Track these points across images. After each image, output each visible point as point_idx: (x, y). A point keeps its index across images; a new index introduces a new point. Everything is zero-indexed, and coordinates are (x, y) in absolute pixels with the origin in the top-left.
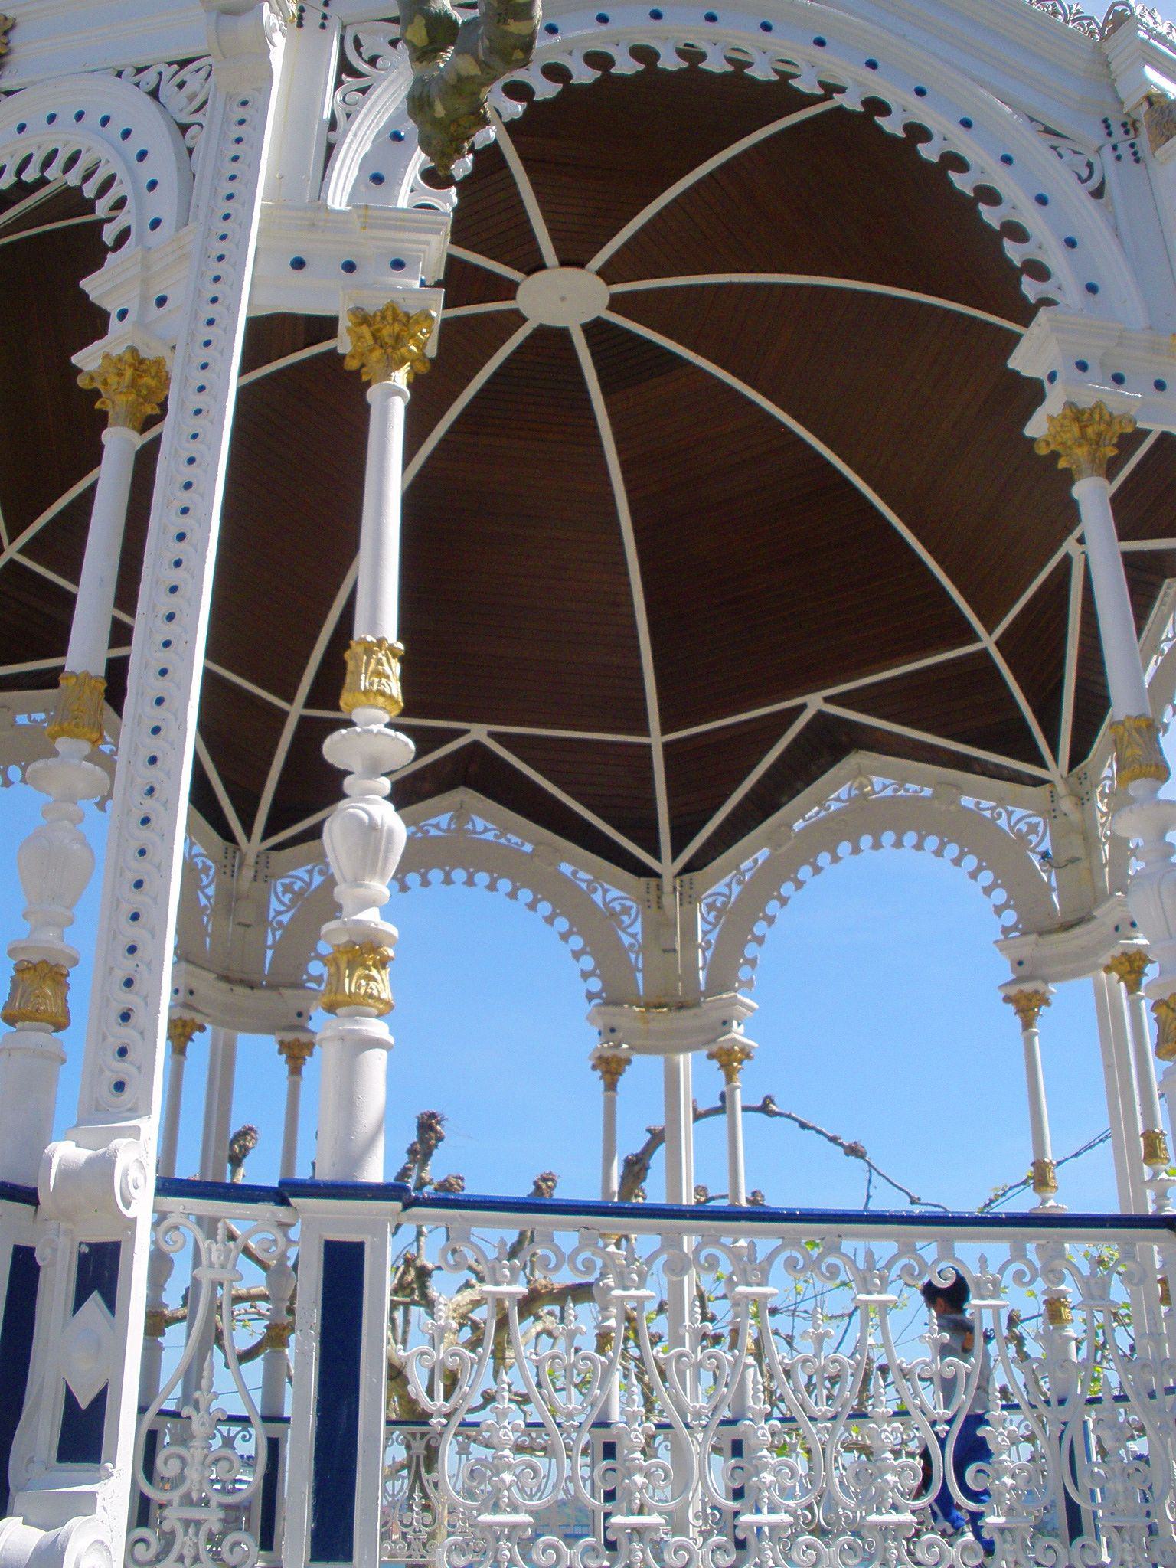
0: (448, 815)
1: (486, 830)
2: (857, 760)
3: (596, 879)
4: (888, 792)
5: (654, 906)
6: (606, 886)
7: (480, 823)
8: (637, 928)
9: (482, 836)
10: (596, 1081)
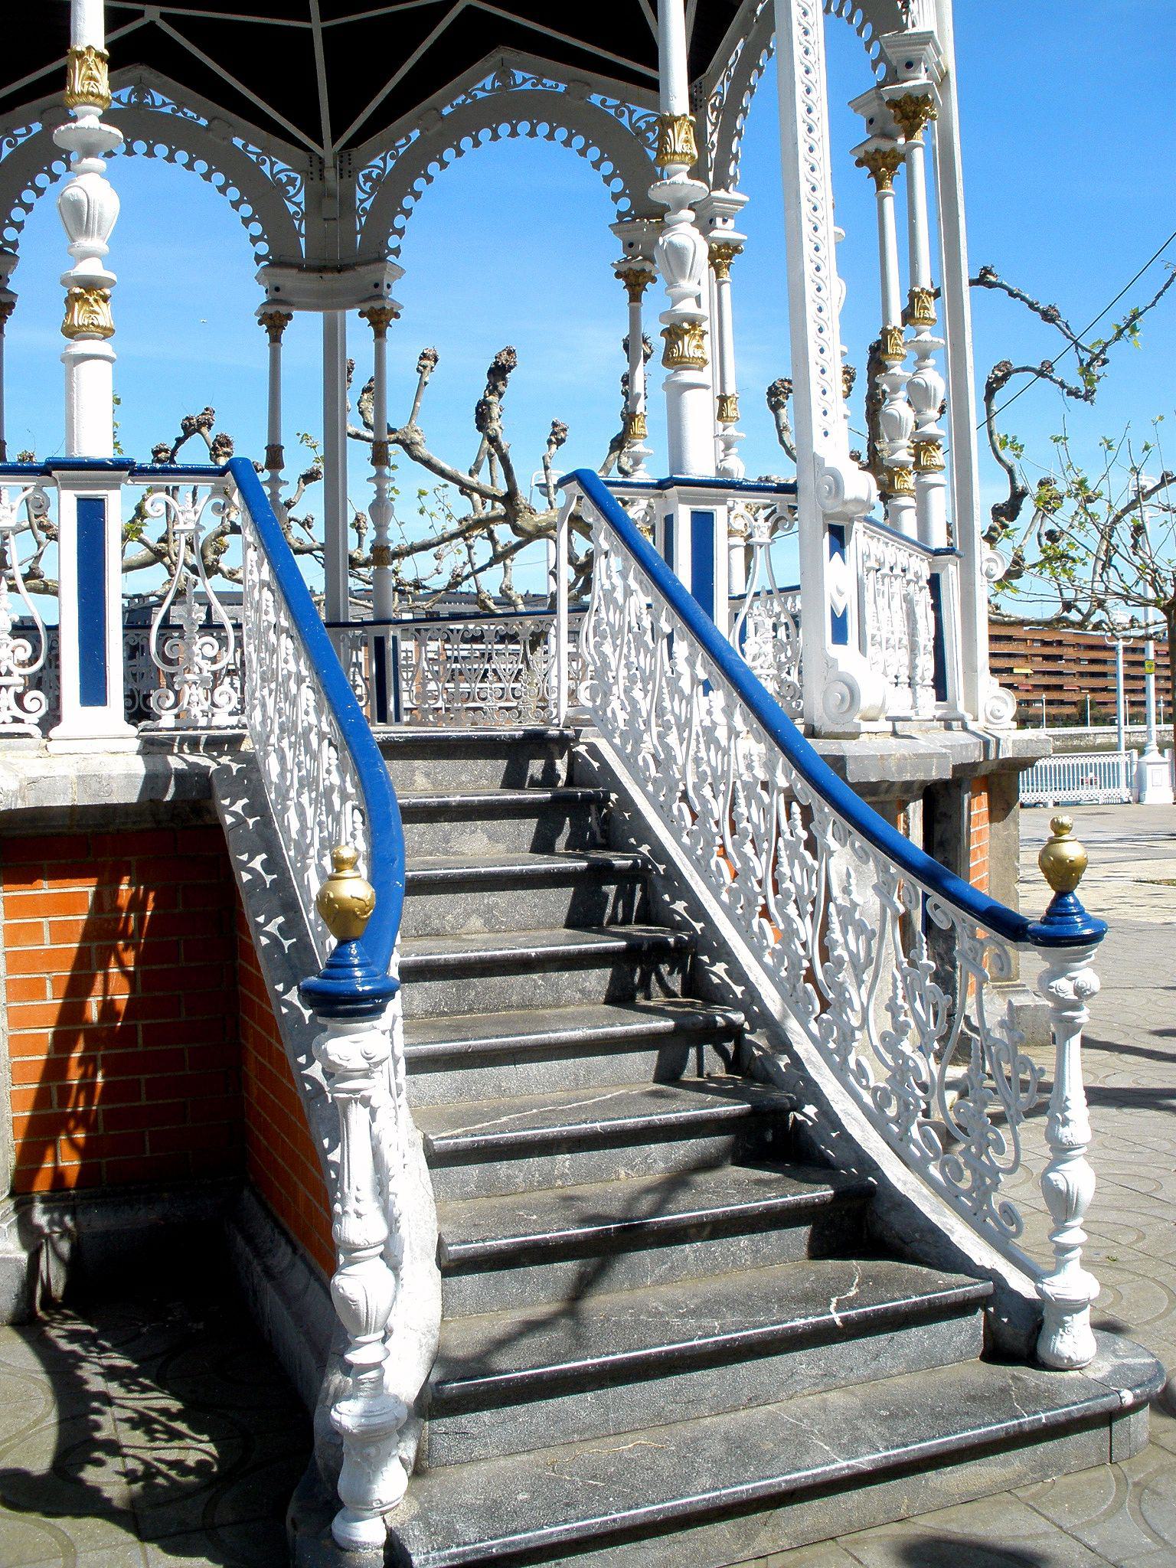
0: (129, 89)
1: (164, 104)
2: (504, 53)
3: (623, 103)
4: (528, 86)
5: (316, 176)
6: (632, 107)
7: (159, 98)
8: (301, 198)
9: (162, 110)
10: (262, 334)
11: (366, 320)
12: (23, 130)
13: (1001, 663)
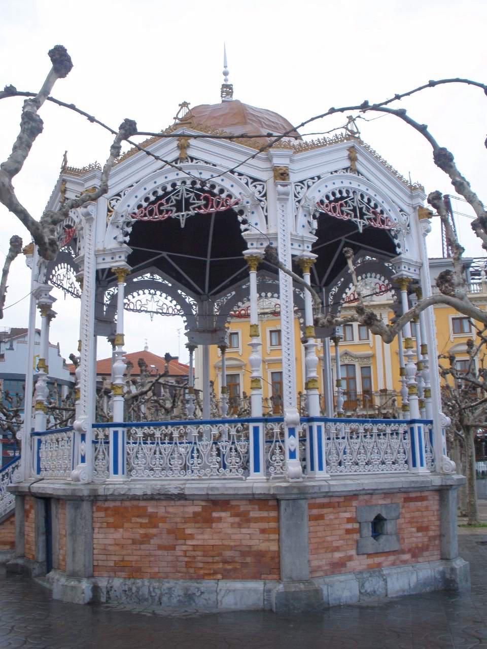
11: (110, 343)
12: (229, 295)
13: (315, 512)
